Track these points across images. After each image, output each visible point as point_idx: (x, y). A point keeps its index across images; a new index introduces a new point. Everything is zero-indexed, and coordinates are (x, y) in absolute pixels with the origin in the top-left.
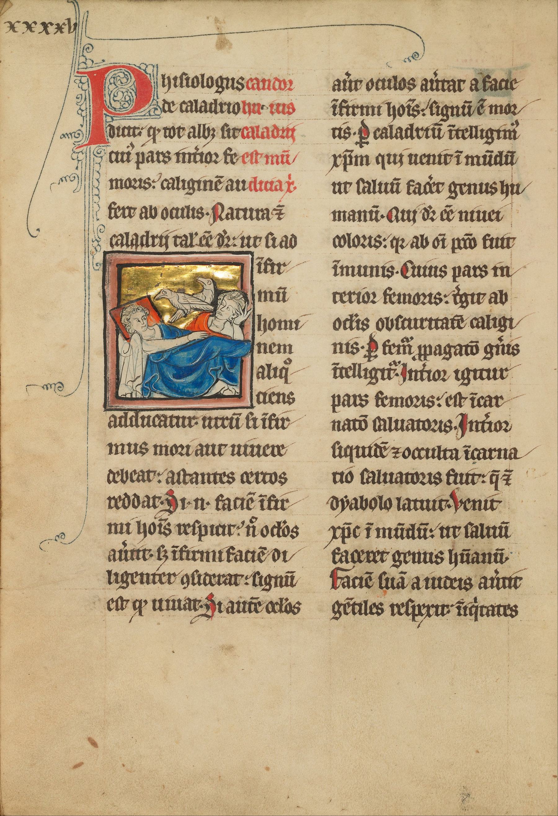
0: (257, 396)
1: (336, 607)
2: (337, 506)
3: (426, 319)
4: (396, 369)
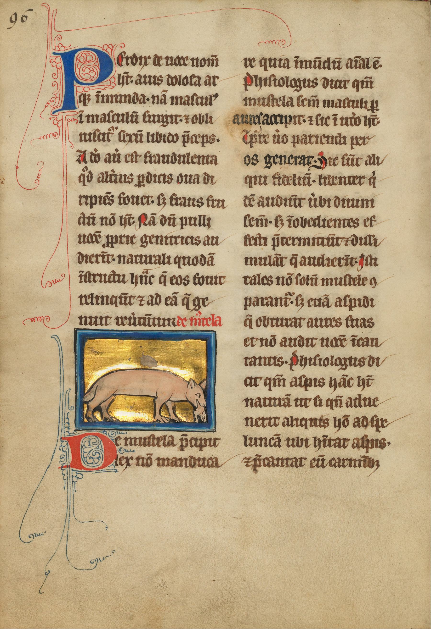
1: (268, 158)
4: (291, 298)
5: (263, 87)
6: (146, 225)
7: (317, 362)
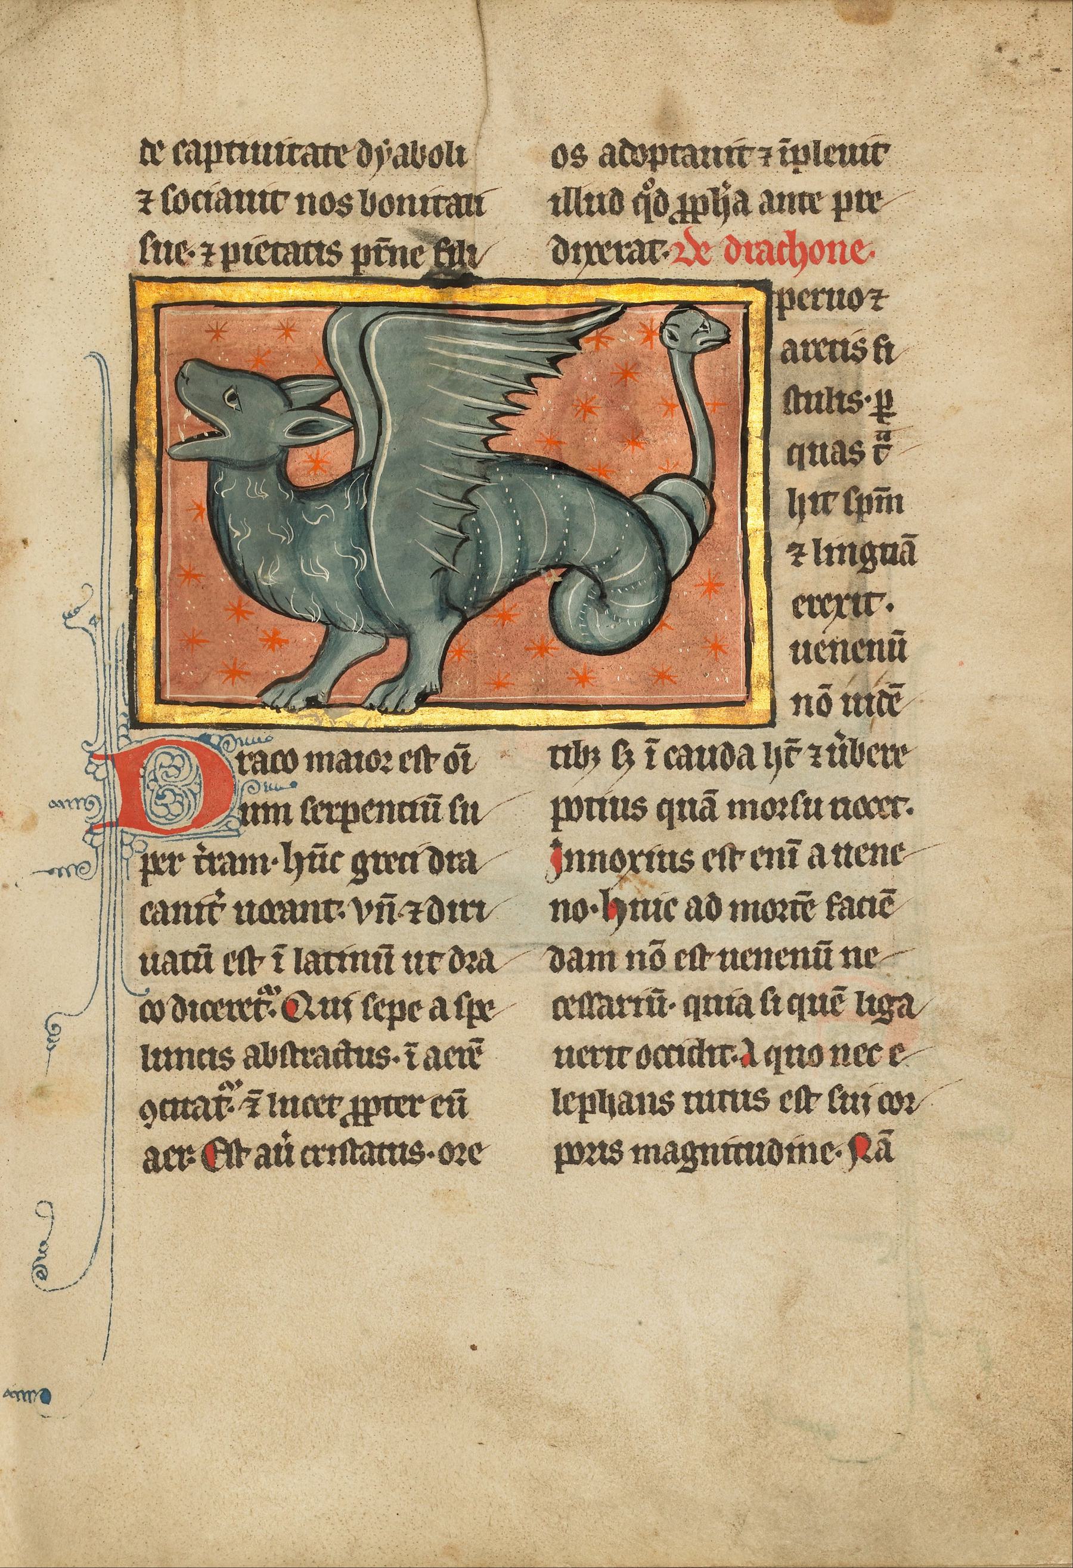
0: (455, 1003)
2: (369, 160)
5: (809, 517)
6: (868, 1160)
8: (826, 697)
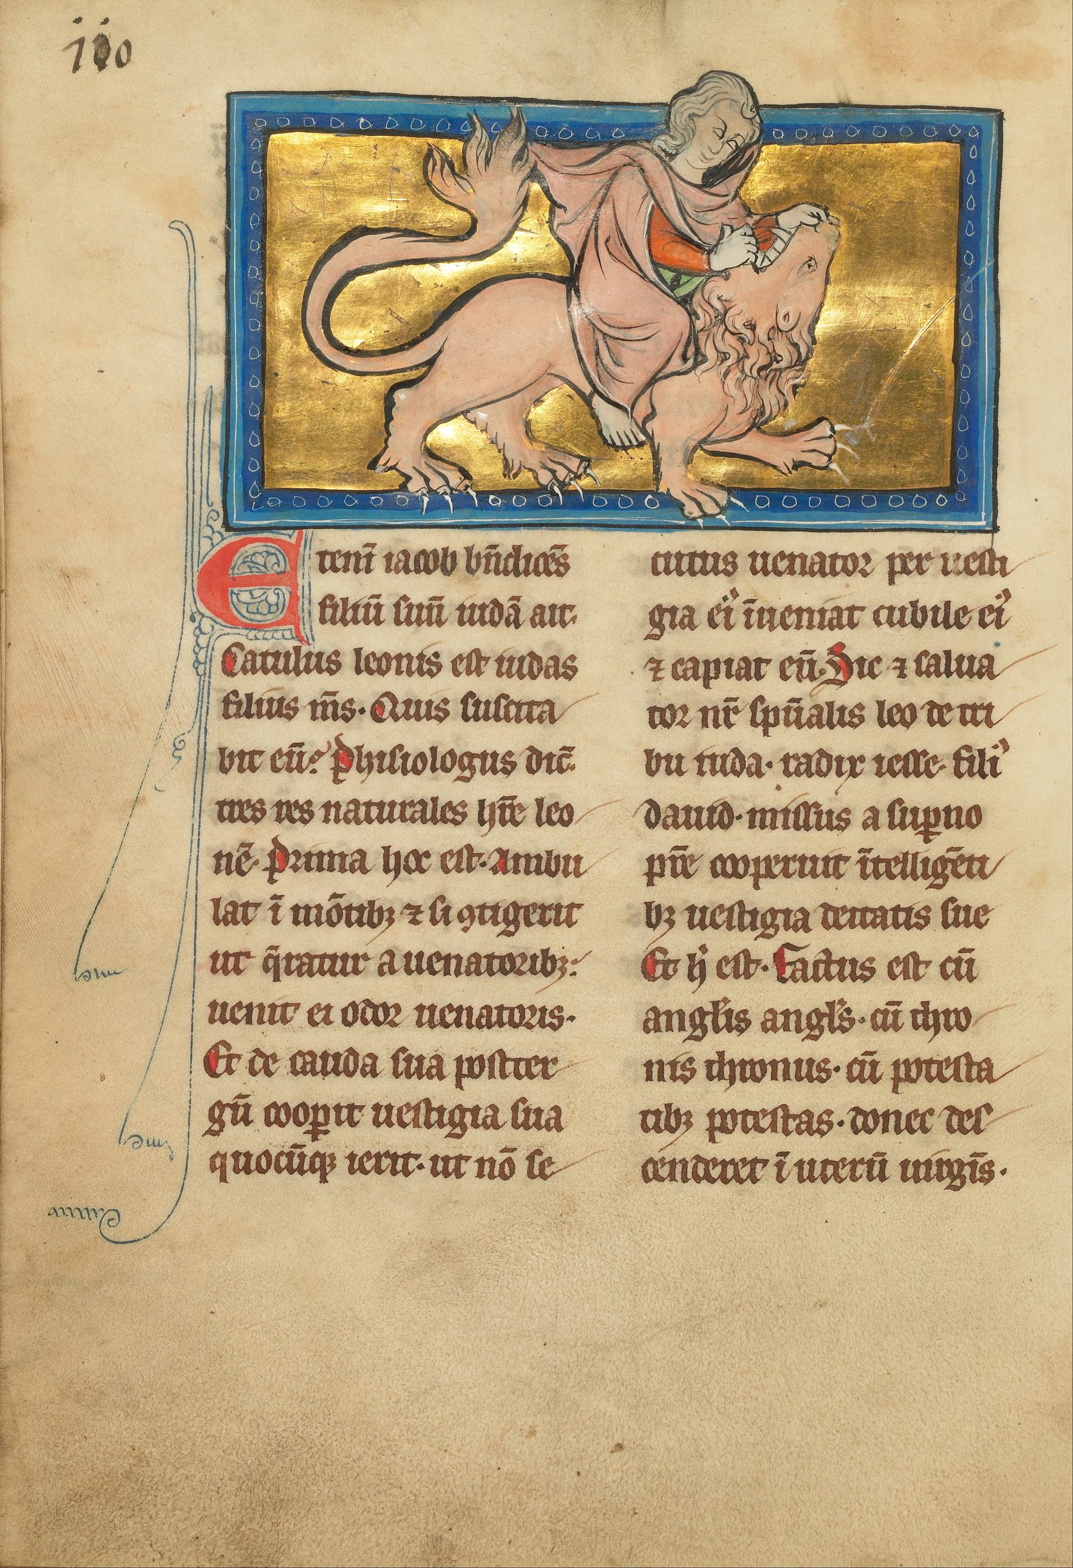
3: (862, 1161)
7: (399, 762)
8: (509, 1161)
